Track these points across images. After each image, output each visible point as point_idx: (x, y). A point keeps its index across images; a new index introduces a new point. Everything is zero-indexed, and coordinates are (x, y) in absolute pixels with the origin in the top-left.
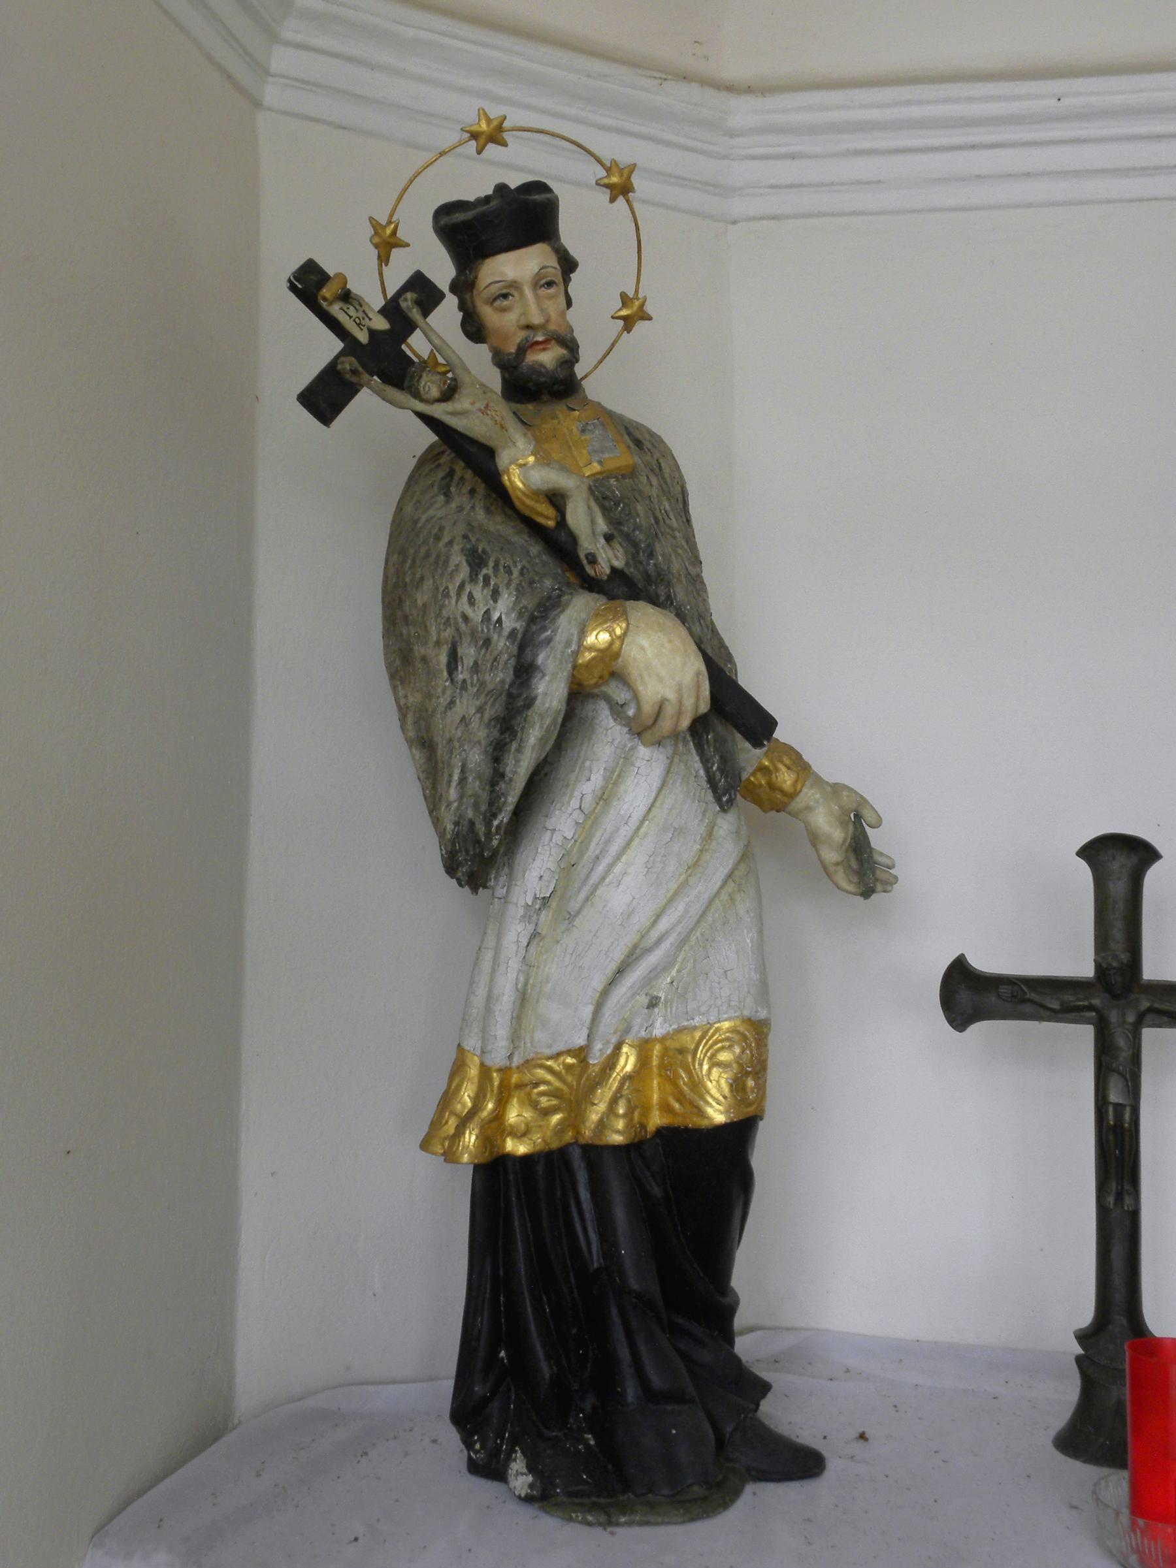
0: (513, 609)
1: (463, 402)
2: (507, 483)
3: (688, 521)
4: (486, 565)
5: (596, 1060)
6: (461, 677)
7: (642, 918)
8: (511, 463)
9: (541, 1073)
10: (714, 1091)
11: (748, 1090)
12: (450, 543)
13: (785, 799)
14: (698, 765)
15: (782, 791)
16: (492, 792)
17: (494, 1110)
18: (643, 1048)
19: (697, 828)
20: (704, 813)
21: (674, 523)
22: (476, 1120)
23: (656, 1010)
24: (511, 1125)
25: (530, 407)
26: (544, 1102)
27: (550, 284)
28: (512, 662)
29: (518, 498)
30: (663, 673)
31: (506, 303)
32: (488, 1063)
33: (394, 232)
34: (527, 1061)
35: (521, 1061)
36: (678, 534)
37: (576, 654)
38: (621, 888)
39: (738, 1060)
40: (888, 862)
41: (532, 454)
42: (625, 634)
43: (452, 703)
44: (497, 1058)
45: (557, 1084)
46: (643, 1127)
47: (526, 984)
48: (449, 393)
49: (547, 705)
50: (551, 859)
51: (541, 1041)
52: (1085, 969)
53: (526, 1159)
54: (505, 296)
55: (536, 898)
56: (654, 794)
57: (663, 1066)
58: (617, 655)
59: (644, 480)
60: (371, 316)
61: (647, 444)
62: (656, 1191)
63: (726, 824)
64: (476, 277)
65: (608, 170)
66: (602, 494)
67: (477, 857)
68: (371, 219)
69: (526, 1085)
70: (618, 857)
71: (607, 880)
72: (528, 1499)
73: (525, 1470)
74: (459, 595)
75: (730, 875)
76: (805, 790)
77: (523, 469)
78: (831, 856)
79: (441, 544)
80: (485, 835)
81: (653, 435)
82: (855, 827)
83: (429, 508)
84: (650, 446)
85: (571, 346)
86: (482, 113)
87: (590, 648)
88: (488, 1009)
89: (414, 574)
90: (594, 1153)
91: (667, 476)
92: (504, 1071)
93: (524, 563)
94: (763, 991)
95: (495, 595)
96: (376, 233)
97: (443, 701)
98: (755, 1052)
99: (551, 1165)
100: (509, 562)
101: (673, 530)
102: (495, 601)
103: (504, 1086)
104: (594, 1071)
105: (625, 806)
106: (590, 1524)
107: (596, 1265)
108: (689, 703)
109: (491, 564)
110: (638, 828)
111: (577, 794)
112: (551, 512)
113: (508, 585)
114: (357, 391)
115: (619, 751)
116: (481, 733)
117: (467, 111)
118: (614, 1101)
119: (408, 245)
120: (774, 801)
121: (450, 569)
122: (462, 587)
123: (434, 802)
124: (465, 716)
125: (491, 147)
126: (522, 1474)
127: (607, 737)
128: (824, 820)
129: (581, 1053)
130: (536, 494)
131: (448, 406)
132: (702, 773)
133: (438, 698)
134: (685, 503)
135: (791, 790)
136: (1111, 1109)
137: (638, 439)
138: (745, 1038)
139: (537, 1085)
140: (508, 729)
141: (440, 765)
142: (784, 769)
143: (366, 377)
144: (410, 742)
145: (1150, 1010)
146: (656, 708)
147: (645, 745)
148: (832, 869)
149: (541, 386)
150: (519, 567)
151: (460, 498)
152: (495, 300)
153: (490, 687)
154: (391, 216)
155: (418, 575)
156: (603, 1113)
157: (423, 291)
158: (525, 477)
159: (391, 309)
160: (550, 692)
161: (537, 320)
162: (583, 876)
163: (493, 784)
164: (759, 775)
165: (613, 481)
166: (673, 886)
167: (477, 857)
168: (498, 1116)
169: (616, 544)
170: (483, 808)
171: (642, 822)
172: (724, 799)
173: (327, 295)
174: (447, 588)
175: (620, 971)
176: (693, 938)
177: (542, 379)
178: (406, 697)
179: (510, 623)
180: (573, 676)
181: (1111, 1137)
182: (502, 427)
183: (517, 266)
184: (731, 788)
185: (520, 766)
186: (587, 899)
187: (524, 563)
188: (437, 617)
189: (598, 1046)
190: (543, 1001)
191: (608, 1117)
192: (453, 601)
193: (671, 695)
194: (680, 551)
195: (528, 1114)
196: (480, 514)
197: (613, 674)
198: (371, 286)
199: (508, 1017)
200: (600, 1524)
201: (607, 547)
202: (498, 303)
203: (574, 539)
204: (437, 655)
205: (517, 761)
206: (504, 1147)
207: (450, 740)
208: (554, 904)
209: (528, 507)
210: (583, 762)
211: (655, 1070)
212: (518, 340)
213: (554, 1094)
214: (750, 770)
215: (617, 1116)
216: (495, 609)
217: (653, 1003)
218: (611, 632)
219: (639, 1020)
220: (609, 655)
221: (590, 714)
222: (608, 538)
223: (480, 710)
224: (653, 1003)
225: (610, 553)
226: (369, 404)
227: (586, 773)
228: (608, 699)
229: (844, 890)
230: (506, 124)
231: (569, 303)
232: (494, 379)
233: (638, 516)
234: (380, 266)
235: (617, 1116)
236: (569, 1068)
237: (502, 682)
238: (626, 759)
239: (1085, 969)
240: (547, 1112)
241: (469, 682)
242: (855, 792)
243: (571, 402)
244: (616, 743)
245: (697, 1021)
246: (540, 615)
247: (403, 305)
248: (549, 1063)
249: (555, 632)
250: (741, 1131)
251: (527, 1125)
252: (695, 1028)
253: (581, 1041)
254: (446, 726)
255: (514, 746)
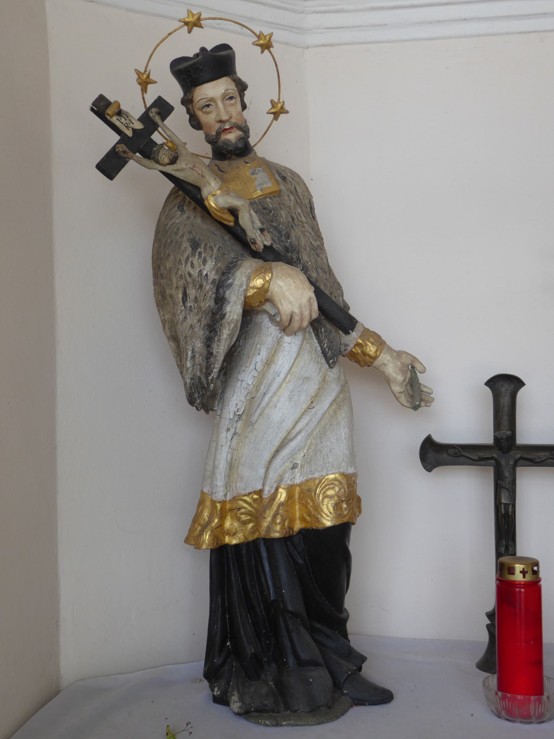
0: (213, 269)
1: (181, 164)
2: (207, 205)
3: (314, 217)
4: (200, 247)
5: (266, 495)
6: (189, 304)
7: (288, 424)
8: (208, 195)
9: (241, 503)
10: (325, 510)
11: (343, 509)
12: (182, 236)
13: (371, 360)
14: (317, 345)
15: (369, 355)
16: (207, 362)
17: (218, 522)
18: (290, 490)
19: (316, 378)
20: (320, 369)
21: (304, 219)
22: (209, 527)
23: (296, 470)
24: (227, 530)
25: (226, 162)
26: (244, 517)
27: (231, 98)
28: (214, 296)
29: (214, 212)
30: (291, 299)
31: (208, 109)
32: (214, 499)
33: (148, 76)
34: (234, 498)
35: (231, 498)
36: (305, 225)
37: (246, 291)
38: (277, 409)
39: (337, 494)
40: (429, 391)
41: (220, 189)
42: (271, 279)
43: (185, 318)
44: (219, 495)
45: (250, 508)
46: (291, 528)
47: (232, 459)
48: (173, 161)
49: (231, 318)
50: (242, 395)
51: (241, 488)
52: (490, 441)
53: (236, 545)
54: (208, 106)
55: (235, 414)
56: (292, 362)
57: (300, 499)
58: (267, 291)
59: (286, 198)
60: (133, 122)
61: (289, 179)
62: (301, 561)
63: (333, 374)
64: (193, 97)
65: (259, 37)
66: (260, 207)
67: (204, 395)
68: (136, 70)
69: (234, 509)
70: (275, 394)
71: (270, 405)
72: (238, 714)
73: (237, 700)
74: (186, 263)
75: (334, 401)
76: (382, 355)
77: (216, 197)
78: (397, 389)
79: (178, 237)
80: (207, 384)
81: (293, 173)
82: (411, 373)
83: (173, 218)
84: (291, 180)
85: (245, 130)
86: (189, 12)
87: (253, 288)
88: (213, 473)
89: (165, 253)
90: (269, 542)
91: (300, 195)
92: (223, 503)
93: (221, 245)
94: (353, 457)
95: (205, 262)
96: (139, 77)
97: (181, 317)
98: (347, 490)
99: (251, 548)
100: (213, 245)
101: (302, 222)
102: (204, 265)
103: (225, 510)
104: (266, 501)
105: (278, 367)
106: (267, 725)
107: (272, 598)
108: (306, 313)
109: (203, 246)
110: (285, 379)
111: (253, 362)
112: (231, 218)
113: (211, 257)
114: (126, 162)
115: (274, 339)
116: (200, 333)
117: (183, 15)
118: (275, 516)
119: (156, 82)
120: (362, 361)
121: (182, 250)
122: (187, 258)
123: (181, 367)
124: (192, 324)
125: (195, 29)
126: (236, 702)
127: (268, 332)
128: (392, 369)
129: (260, 492)
130: (222, 209)
131: (174, 167)
132: (319, 348)
133: (179, 315)
134: (312, 209)
135: (374, 355)
136: (503, 506)
137: (283, 175)
138: (341, 483)
139: (239, 509)
140: (213, 330)
141: (182, 349)
142: (370, 344)
143: (131, 154)
144: (168, 338)
145: (521, 458)
146: (289, 317)
147: (288, 335)
148: (398, 395)
149: (232, 151)
150: (217, 247)
151: (188, 213)
152: (203, 108)
153: (203, 309)
154: (146, 68)
155: (167, 253)
156: (269, 523)
157: (163, 108)
158: (215, 201)
159: (145, 118)
160: (234, 311)
161: (225, 117)
162: (258, 403)
163: (208, 358)
164: (357, 348)
165: (268, 200)
166: (304, 407)
167: (204, 395)
168: (221, 525)
169: (266, 233)
170: (204, 371)
171: (287, 375)
172: (331, 362)
173: (110, 113)
174: (180, 259)
175: (277, 451)
176: (315, 433)
177: (230, 149)
178: (164, 315)
179: (212, 276)
180: (245, 302)
181: (503, 520)
182: (202, 176)
183: (214, 90)
184: (335, 356)
185: (220, 349)
186: (260, 415)
187: (221, 245)
188: (176, 275)
189: (267, 489)
190: (240, 467)
191: (272, 524)
192: (184, 266)
193: (297, 310)
194: (307, 234)
195: (236, 524)
196: (199, 220)
197: (267, 300)
198: (134, 105)
199: (223, 475)
200: (273, 726)
201: (261, 235)
202: (204, 110)
203: (243, 231)
204: (177, 294)
205: (218, 346)
206: (225, 541)
207: (186, 337)
208: (244, 417)
209: (218, 216)
210: (257, 345)
211: (297, 500)
212: (216, 129)
213: (248, 513)
214: (352, 345)
215: (276, 524)
216: (204, 269)
217: (294, 467)
218: (264, 279)
219: (287, 475)
220: (263, 291)
221: (260, 321)
222: (262, 230)
223: (199, 321)
224: (294, 467)
225: (263, 238)
226: (133, 167)
227: (258, 351)
228: (266, 312)
229: (405, 406)
230: (202, 17)
231: (244, 107)
232: (208, 150)
233: (282, 217)
234: (143, 94)
235: (276, 524)
236: (255, 500)
237: (209, 306)
238: (279, 342)
239: (490, 441)
240: (245, 523)
241: (193, 307)
242: (410, 355)
243: (246, 159)
244: (273, 335)
245: (316, 475)
246: (227, 272)
247: (151, 115)
248: (245, 498)
249: (234, 280)
250: (342, 531)
251: (236, 529)
252: (315, 479)
253: (259, 487)
254: (183, 330)
255: (216, 339)
